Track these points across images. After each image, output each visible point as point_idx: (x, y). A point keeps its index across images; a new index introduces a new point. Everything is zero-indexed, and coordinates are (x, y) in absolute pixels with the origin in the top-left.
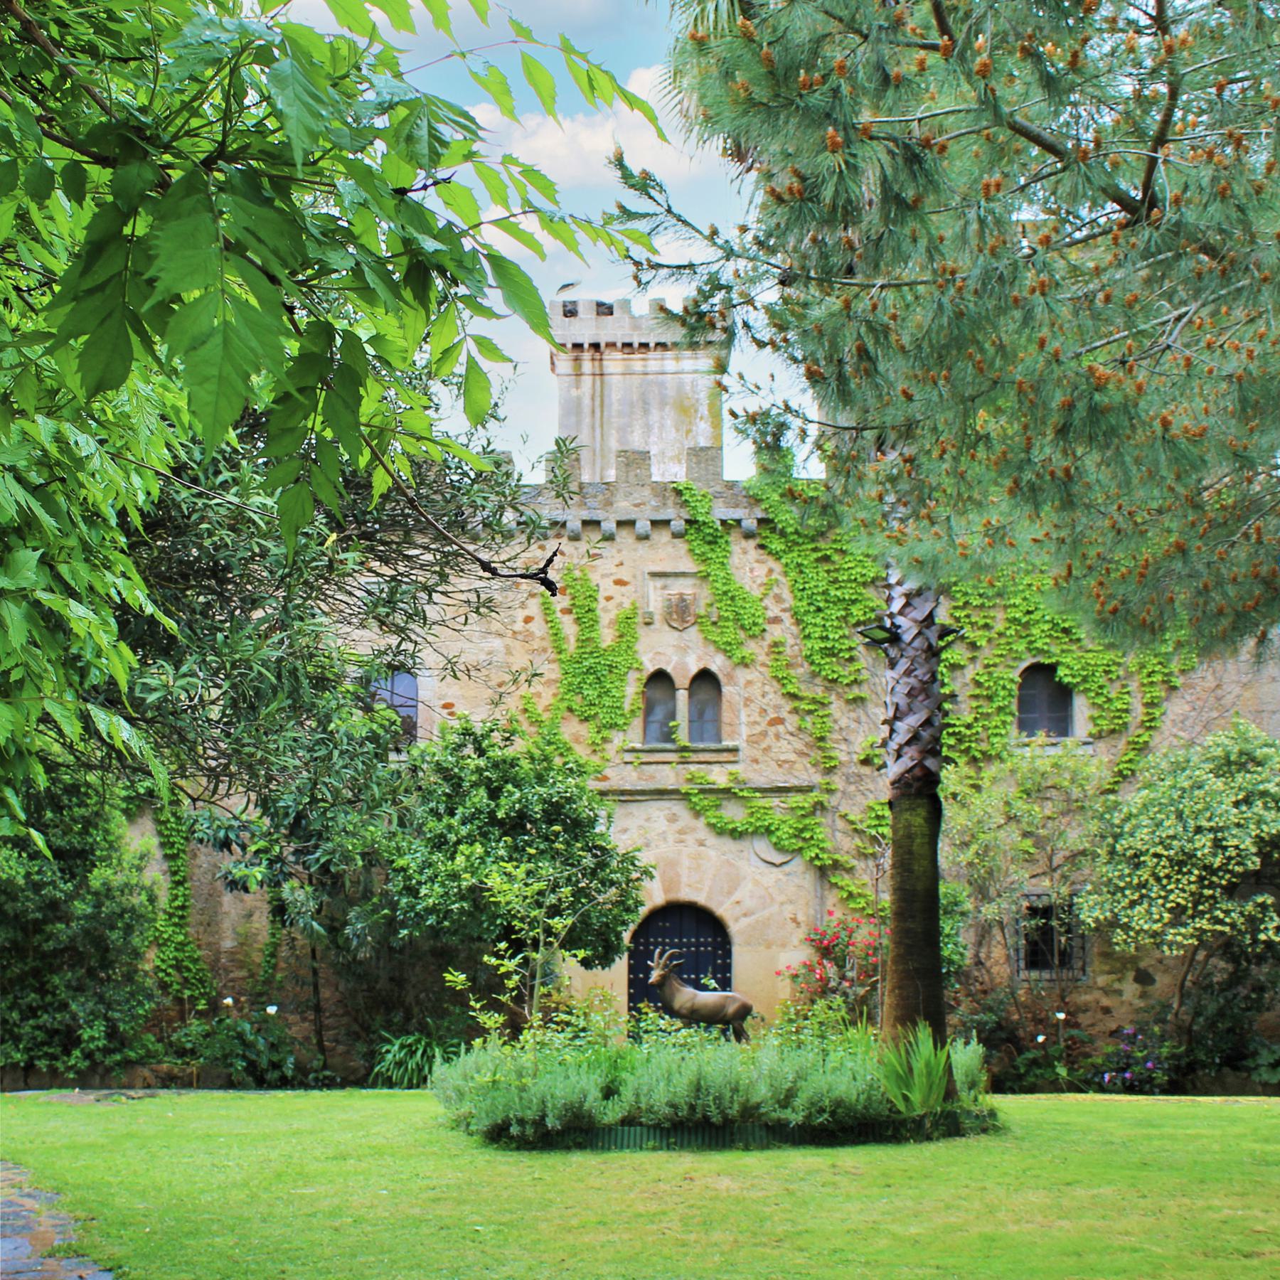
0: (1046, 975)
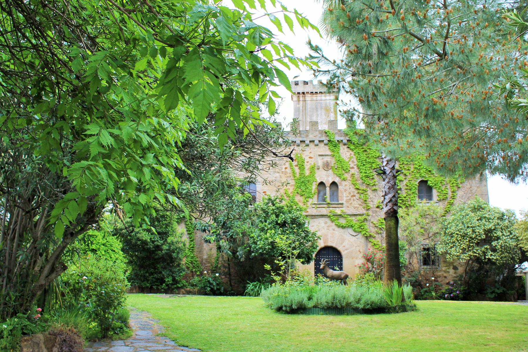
0: (428, 267)
